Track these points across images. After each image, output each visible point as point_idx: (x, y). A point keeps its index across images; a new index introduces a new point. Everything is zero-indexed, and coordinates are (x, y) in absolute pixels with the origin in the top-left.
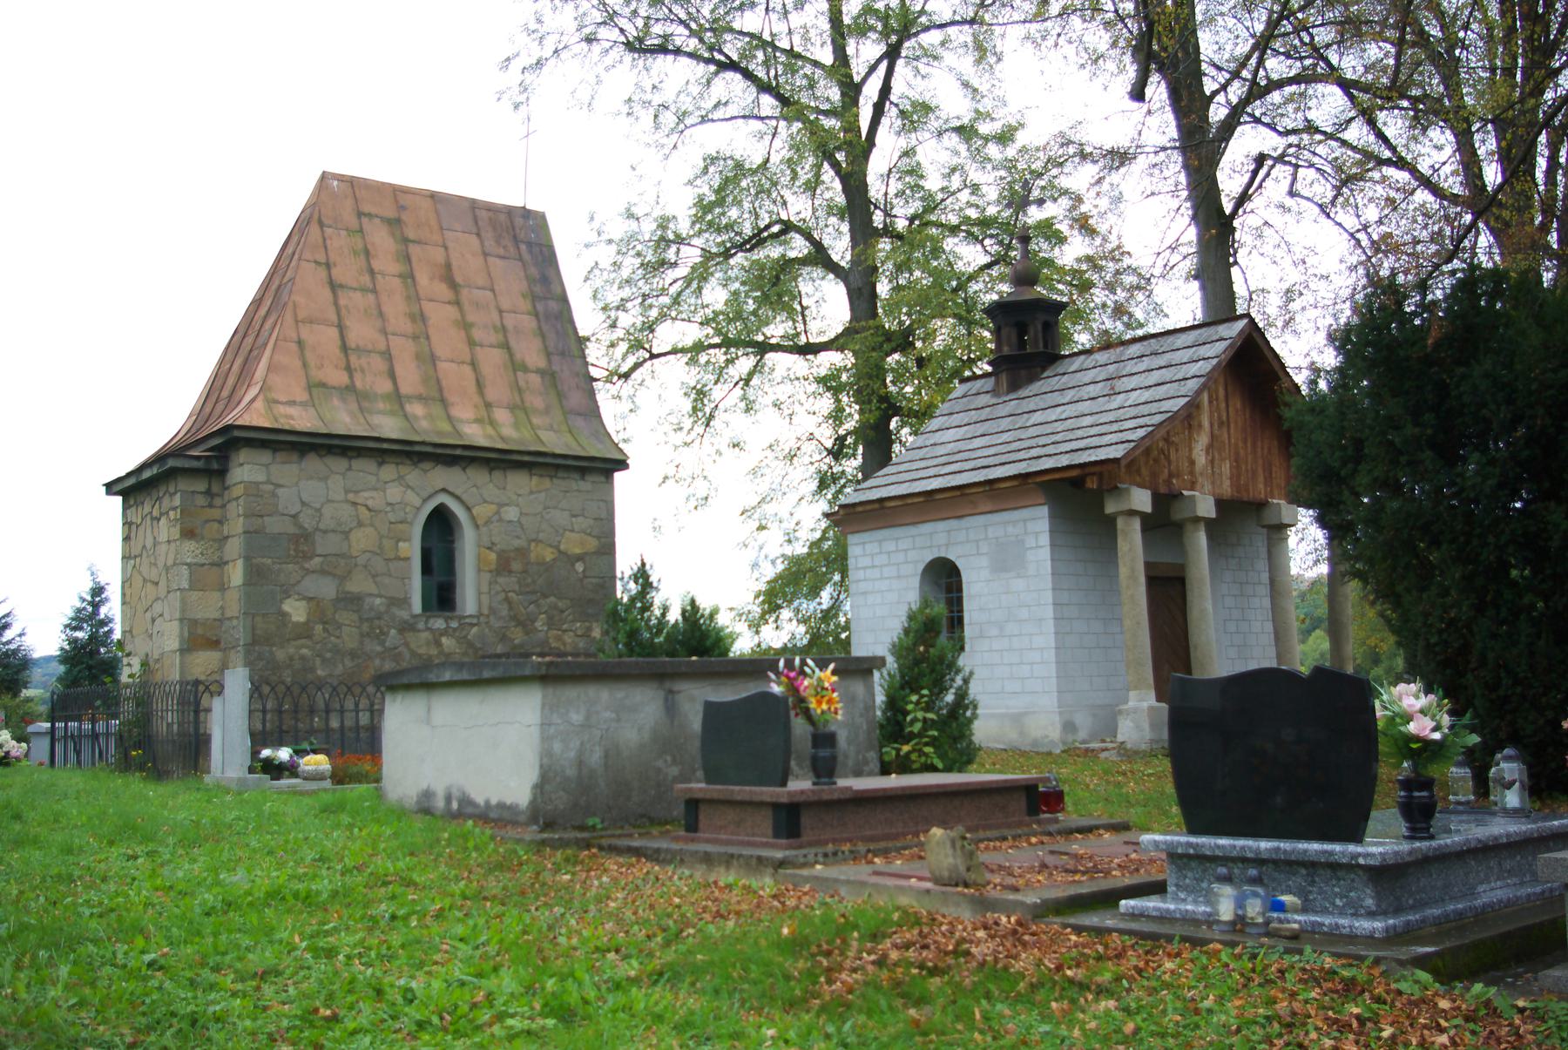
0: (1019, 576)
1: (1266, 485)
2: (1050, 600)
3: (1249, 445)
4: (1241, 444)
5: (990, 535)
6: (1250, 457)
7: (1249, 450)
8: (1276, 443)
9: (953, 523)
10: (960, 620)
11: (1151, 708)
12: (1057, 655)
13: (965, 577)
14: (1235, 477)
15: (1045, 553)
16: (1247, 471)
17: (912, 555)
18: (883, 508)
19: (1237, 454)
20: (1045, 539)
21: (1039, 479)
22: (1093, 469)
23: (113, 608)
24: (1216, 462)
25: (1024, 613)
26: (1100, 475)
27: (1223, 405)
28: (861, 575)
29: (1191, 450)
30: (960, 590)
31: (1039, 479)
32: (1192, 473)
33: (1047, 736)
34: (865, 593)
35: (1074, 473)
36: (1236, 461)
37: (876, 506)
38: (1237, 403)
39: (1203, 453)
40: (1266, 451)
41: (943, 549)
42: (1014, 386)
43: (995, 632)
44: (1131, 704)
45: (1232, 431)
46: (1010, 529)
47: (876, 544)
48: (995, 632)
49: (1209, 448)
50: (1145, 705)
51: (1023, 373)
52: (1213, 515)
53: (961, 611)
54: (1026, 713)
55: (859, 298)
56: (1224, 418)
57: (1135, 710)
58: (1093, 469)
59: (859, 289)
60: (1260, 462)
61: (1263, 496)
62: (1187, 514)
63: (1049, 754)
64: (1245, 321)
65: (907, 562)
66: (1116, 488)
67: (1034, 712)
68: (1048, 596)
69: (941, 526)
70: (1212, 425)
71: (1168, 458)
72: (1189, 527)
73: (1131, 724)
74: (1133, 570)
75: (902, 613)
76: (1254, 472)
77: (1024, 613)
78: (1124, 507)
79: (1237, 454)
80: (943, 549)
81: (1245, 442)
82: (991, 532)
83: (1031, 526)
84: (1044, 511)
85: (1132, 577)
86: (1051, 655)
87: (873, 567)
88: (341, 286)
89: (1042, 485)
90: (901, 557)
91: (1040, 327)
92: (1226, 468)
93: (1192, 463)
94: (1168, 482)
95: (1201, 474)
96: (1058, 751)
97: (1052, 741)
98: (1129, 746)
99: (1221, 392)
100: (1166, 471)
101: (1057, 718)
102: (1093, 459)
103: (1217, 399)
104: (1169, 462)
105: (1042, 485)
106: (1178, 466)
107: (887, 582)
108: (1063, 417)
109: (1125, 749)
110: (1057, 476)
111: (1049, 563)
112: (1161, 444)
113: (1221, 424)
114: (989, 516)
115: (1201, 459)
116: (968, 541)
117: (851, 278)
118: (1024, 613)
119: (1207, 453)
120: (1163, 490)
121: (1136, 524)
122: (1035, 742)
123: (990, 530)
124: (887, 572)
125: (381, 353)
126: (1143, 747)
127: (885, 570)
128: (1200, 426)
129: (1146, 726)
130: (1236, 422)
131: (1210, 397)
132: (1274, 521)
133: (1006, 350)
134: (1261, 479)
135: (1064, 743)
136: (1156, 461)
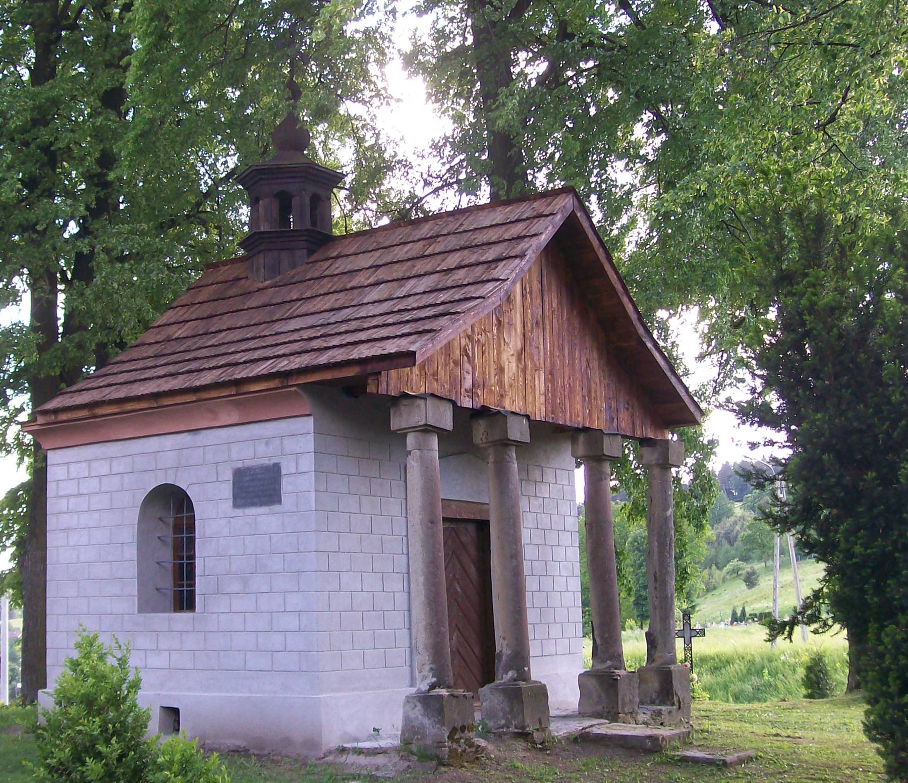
6: (567, 370)
8: (595, 355)
10: (192, 568)
13: (200, 511)
16: (563, 387)
19: (553, 365)
21: (302, 380)
24: (528, 371)
25: (276, 563)
28: (63, 504)
30: (192, 528)
31: (302, 380)
32: (500, 383)
34: (67, 529)
38: (553, 300)
39: (513, 360)
40: (584, 364)
41: (171, 473)
45: (548, 337)
47: (84, 465)
48: (236, 587)
49: (520, 355)
53: (193, 557)
60: (578, 375)
69: (168, 442)
75: (421, 560)
77: (276, 563)
79: (553, 365)
80: (171, 473)
81: (562, 349)
83: (290, 445)
84: (309, 423)
87: (80, 495)
88: (177, 471)
89: (307, 387)
93: (501, 370)
99: (536, 286)
100: (469, 378)
102: (379, 352)
105: (307, 387)
107: (96, 515)
108: (337, 306)
110: (328, 376)
112: (463, 342)
113: (537, 323)
115: (511, 367)
119: (519, 359)
125: (111, 461)
131: (523, 289)
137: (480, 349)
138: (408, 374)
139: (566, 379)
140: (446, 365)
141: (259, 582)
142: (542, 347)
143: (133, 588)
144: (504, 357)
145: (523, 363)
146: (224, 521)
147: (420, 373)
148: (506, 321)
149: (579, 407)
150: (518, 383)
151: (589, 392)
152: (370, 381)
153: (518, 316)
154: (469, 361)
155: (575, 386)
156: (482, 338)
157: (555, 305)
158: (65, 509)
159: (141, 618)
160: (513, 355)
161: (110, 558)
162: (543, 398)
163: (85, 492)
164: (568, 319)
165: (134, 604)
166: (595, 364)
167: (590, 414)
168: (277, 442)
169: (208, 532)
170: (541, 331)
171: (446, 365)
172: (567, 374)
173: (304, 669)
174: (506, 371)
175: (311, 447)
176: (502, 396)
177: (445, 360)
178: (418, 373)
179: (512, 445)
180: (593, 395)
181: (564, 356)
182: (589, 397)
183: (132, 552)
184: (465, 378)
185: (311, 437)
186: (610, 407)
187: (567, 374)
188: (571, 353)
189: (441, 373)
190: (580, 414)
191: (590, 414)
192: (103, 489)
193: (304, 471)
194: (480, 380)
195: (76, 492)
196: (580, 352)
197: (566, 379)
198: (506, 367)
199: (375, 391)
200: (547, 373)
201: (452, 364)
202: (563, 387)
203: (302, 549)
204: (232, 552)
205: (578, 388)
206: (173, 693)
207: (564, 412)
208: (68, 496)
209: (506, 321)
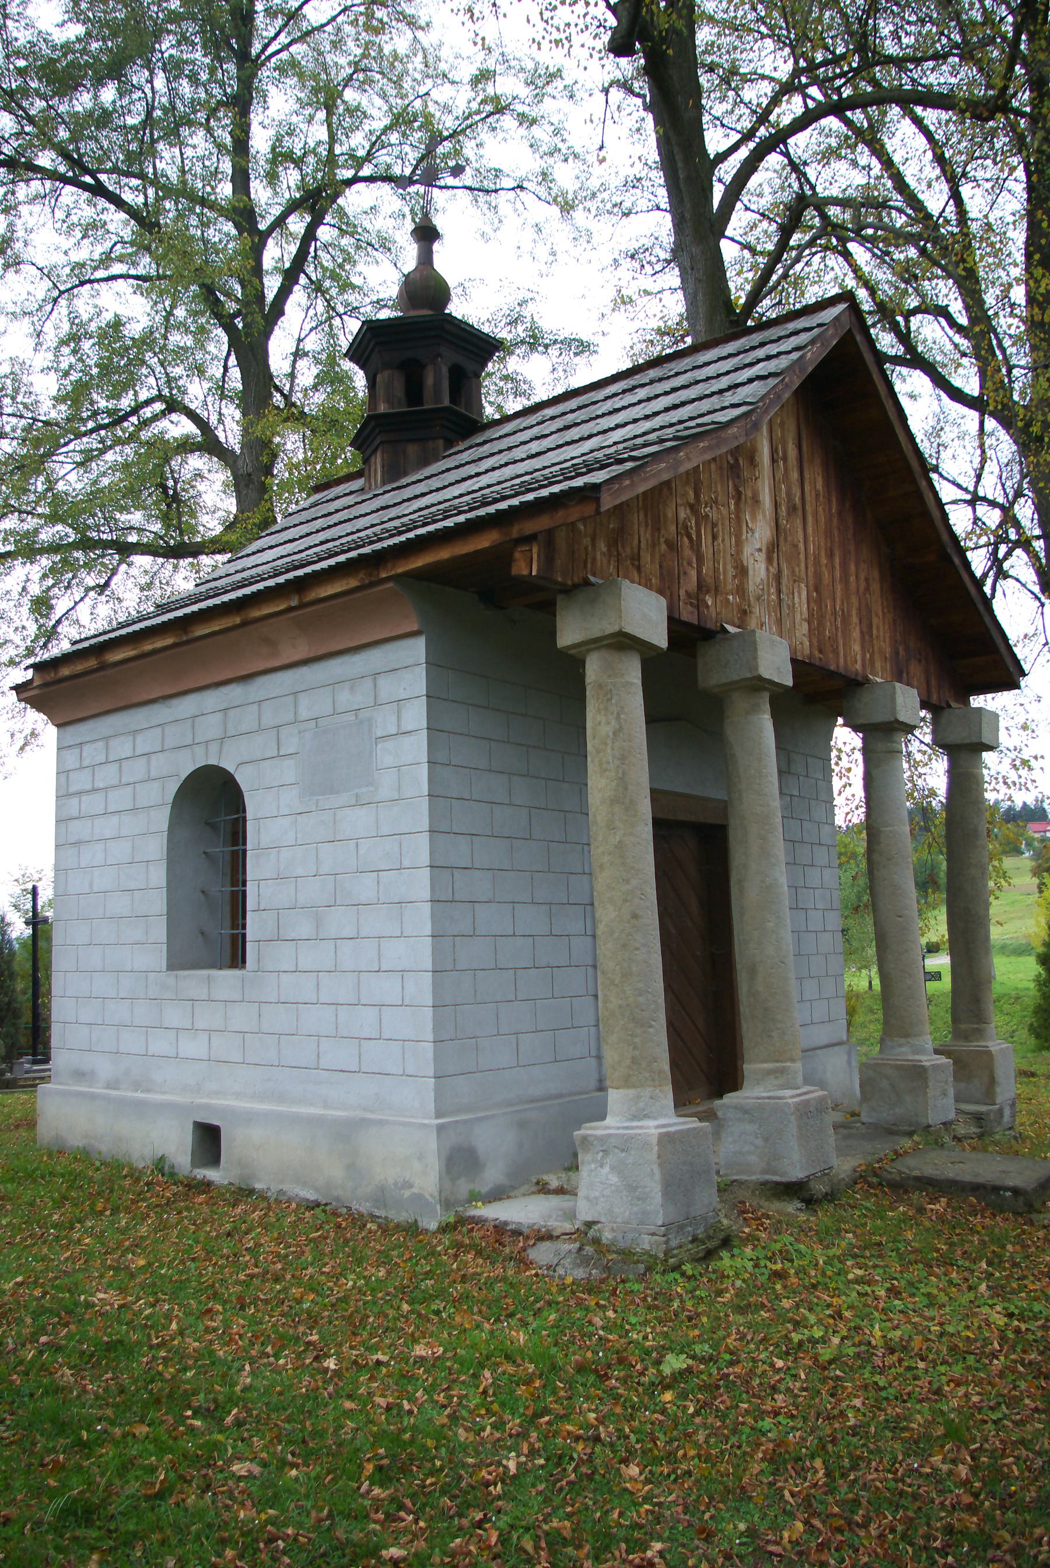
0: (359, 803)
1: (863, 648)
2: (425, 858)
3: (837, 561)
4: (824, 561)
5: (304, 713)
6: (839, 588)
7: (838, 574)
8: (876, 574)
9: (234, 693)
11: (667, 1139)
12: (436, 986)
14: (816, 621)
15: (417, 748)
16: (834, 613)
17: (160, 764)
18: (103, 667)
19: (818, 576)
20: (416, 715)
22: (530, 526)
23: (46, 894)
24: (784, 581)
26: (548, 538)
27: (795, 475)
29: (739, 544)
32: (741, 591)
33: (408, 1185)
35: (484, 542)
36: (817, 589)
37: (92, 663)
38: (816, 480)
39: (761, 557)
40: (863, 585)
41: (214, 747)
42: (394, 472)
43: (304, 928)
44: (613, 1124)
45: (810, 530)
46: (345, 698)
48: (304, 928)
49: (772, 550)
50: (651, 1128)
51: (412, 449)
52: (790, 682)
54: (364, 1123)
55: (247, 486)
56: (797, 500)
57: (626, 1144)
58: (530, 526)
59: (249, 475)
61: (858, 666)
62: (736, 673)
63: (412, 1229)
64: (842, 307)
65: (149, 779)
66: (587, 583)
67: (381, 1123)
68: (420, 849)
69: (212, 699)
70: (776, 506)
71: (696, 546)
72: (739, 703)
73: (614, 1179)
74: (623, 781)
76: (846, 620)
77: (365, 888)
78: (603, 626)
79: (818, 576)
80: (214, 747)
81: (831, 556)
82: (306, 708)
83: (388, 687)
84: (417, 649)
85: (621, 799)
86: (421, 989)
87: (95, 790)
90: (136, 770)
91: (445, 371)
92: (801, 599)
93: (742, 571)
94: (699, 604)
95: (758, 598)
96: (433, 1226)
97: (418, 1198)
98: (607, 1236)
99: (792, 452)
101: (432, 1144)
103: (785, 459)
104: (700, 559)
106: (716, 570)
107: (115, 819)
109: (596, 1241)
111: (423, 771)
113: (792, 509)
114: (304, 671)
115: (759, 570)
116: (260, 730)
117: (240, 463)
118: (365, 888)
119: (769, 560)
120: (687, 614)
121: (632, 671)
122: (381, 1196)
123: (304, 701)
124: (120, 799)
126: (646, 1243)
127: (113, 795)
128: (756, 501)
129: (654, 1188)
130: (816, 515)
132: (880, 716)
133: (382, 408)
134: (856, 634)
135: (447, 1204)
136: (672, 546)
137: (709, 530)
138: (586, 548)
139: (838, 602)
140: (654, 545)
141: (340, 921)
142: (801, 546)
143: (160, 932)
144: (747, 550)
145: (775, 564)
146: (286, 822)
147: (609, 550)
148: (749, 494)
149: (856, 647)
150: (769, 595)
151: (870, 627)
152: (517, 555)
153: (767, 490)
154: (692, 548)
155: (850, 615)
156: (714, 515)
157: (820, 486)
158: (76, 814)
159: (170, 978)
160: (760, 550)
161: (132, 885)
162: (805, 625)
163: (101, 786)
164: (840, 513)
165: (158, 958)
166: (876, 587)
167: (872, 659)
168: (368, 683)
169: (265, 840)
170: (799, 522)
171: (654, 545)
172: (838, 594)
173: (409, 1072)
174: (751, 573)
175: (421, 687)
176: (745, 612)
177: (652, 535)
178: (604, 549)
179: (766, 689)
180: (875, 632)
181: (833, 567)
182: (867, 635)
183: (158, 875)
184: (685, 573)
185: (421, 672)
186: (898, 654)
187: (838, 594)
188: (844, 565)
189: (646, 558)
190: (859, 658)
191: (872, 659)
192: (124, 780)
193: (410, 728)
194: (710, 581)
195: (89, 787)
196: (857, 565)
197: (838, 602)
198: (751, 567)
199: (525, 572)
200: (811, 588)
201: (664, 547)
202: (835, 613)
203: (406, 863)
204: (300, 871)
205: (855, 619)
206: (213, 1102)
207: (836, 652)
208: (80, 793)
209: (749, 494)
